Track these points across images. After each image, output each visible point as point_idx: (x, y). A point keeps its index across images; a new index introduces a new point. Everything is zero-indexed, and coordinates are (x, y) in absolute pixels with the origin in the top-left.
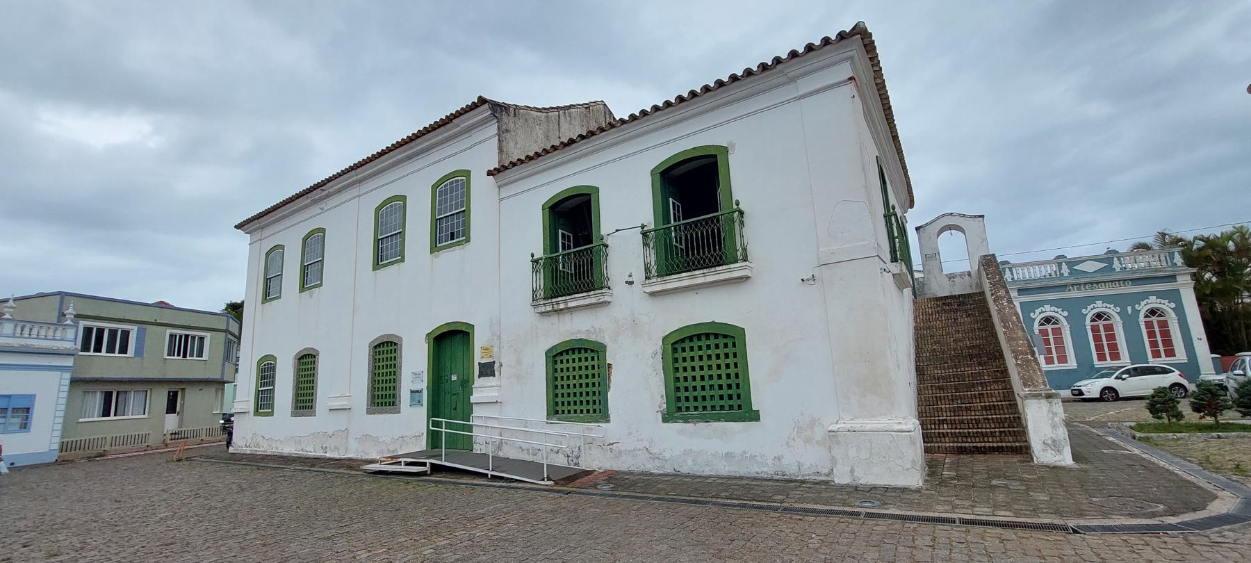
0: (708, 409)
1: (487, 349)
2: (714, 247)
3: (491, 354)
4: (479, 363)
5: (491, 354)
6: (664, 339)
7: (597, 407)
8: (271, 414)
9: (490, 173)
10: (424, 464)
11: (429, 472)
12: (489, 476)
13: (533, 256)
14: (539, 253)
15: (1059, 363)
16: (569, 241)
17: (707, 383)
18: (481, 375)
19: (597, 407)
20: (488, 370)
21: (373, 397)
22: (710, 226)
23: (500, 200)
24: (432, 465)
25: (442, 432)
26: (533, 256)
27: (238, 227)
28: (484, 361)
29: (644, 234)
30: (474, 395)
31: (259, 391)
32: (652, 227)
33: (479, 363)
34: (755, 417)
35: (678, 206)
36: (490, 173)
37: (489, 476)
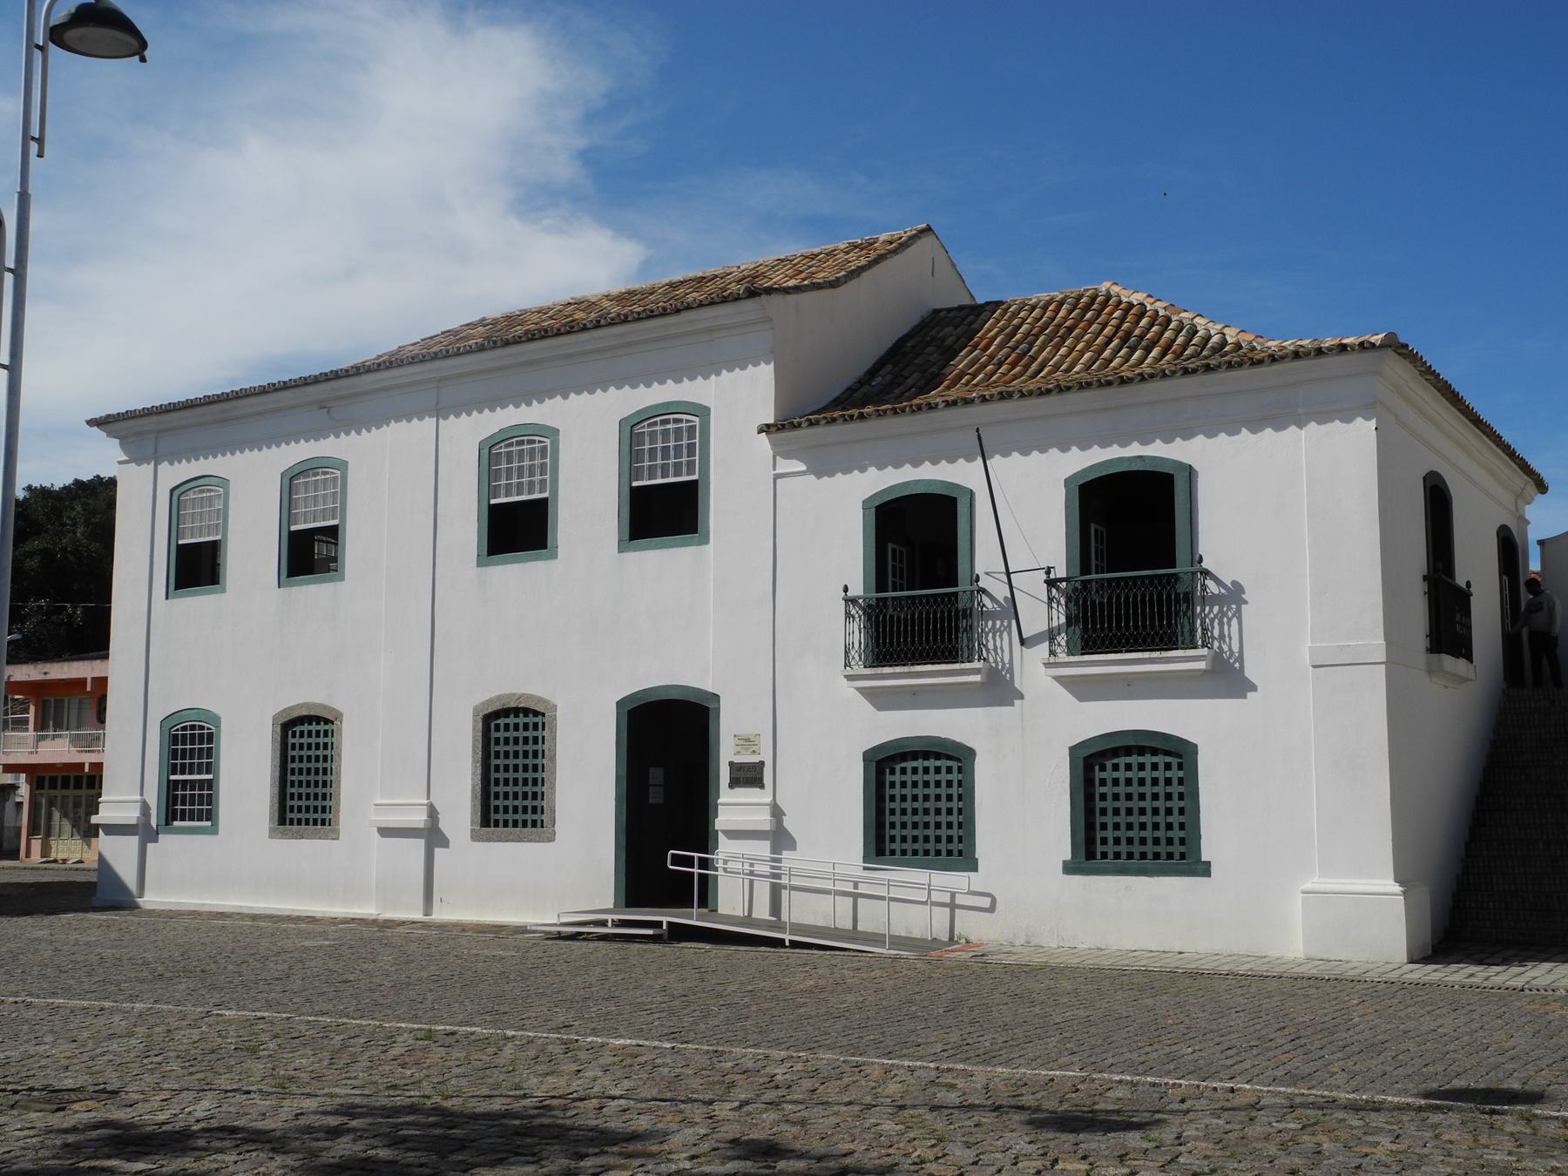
0: (1148, 857)
1: (748, 740)
2: (1161, 621)
3: (755, 748)
4: (731, 764)
5: (755, 748)
6: (283, 475)
7: (954, 846)
8: (214, 831)
9: (765, 429)
10: (658, 924)
11: (666, 937)
12: (787, 944)
13: (846, 589)
14: (857, 590)
15: (662, 922)
16: (902, 578)
17: (920, 791)
18: (734, 783)
19: (954, 846)
20: (748, 776)
21: (210, 800)
22: (1157, 588)
23: (777, 477)
24: (669, 923)
25: (693, 873)
26: (846, 589)
27: (93, 422)
28: (738, 759)
29: (1051, 583)
30: (719, 818)
31: (169, 781)
32: (861, 593)
33: (731, 764)
34: (1204, 870)
35: (1102, 533)
36: (765, 429)
37: (787, 944)
